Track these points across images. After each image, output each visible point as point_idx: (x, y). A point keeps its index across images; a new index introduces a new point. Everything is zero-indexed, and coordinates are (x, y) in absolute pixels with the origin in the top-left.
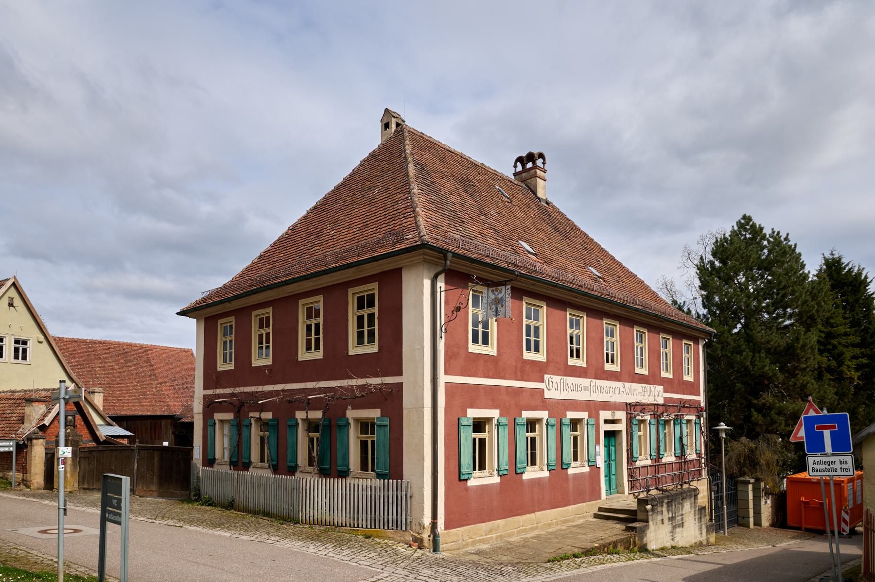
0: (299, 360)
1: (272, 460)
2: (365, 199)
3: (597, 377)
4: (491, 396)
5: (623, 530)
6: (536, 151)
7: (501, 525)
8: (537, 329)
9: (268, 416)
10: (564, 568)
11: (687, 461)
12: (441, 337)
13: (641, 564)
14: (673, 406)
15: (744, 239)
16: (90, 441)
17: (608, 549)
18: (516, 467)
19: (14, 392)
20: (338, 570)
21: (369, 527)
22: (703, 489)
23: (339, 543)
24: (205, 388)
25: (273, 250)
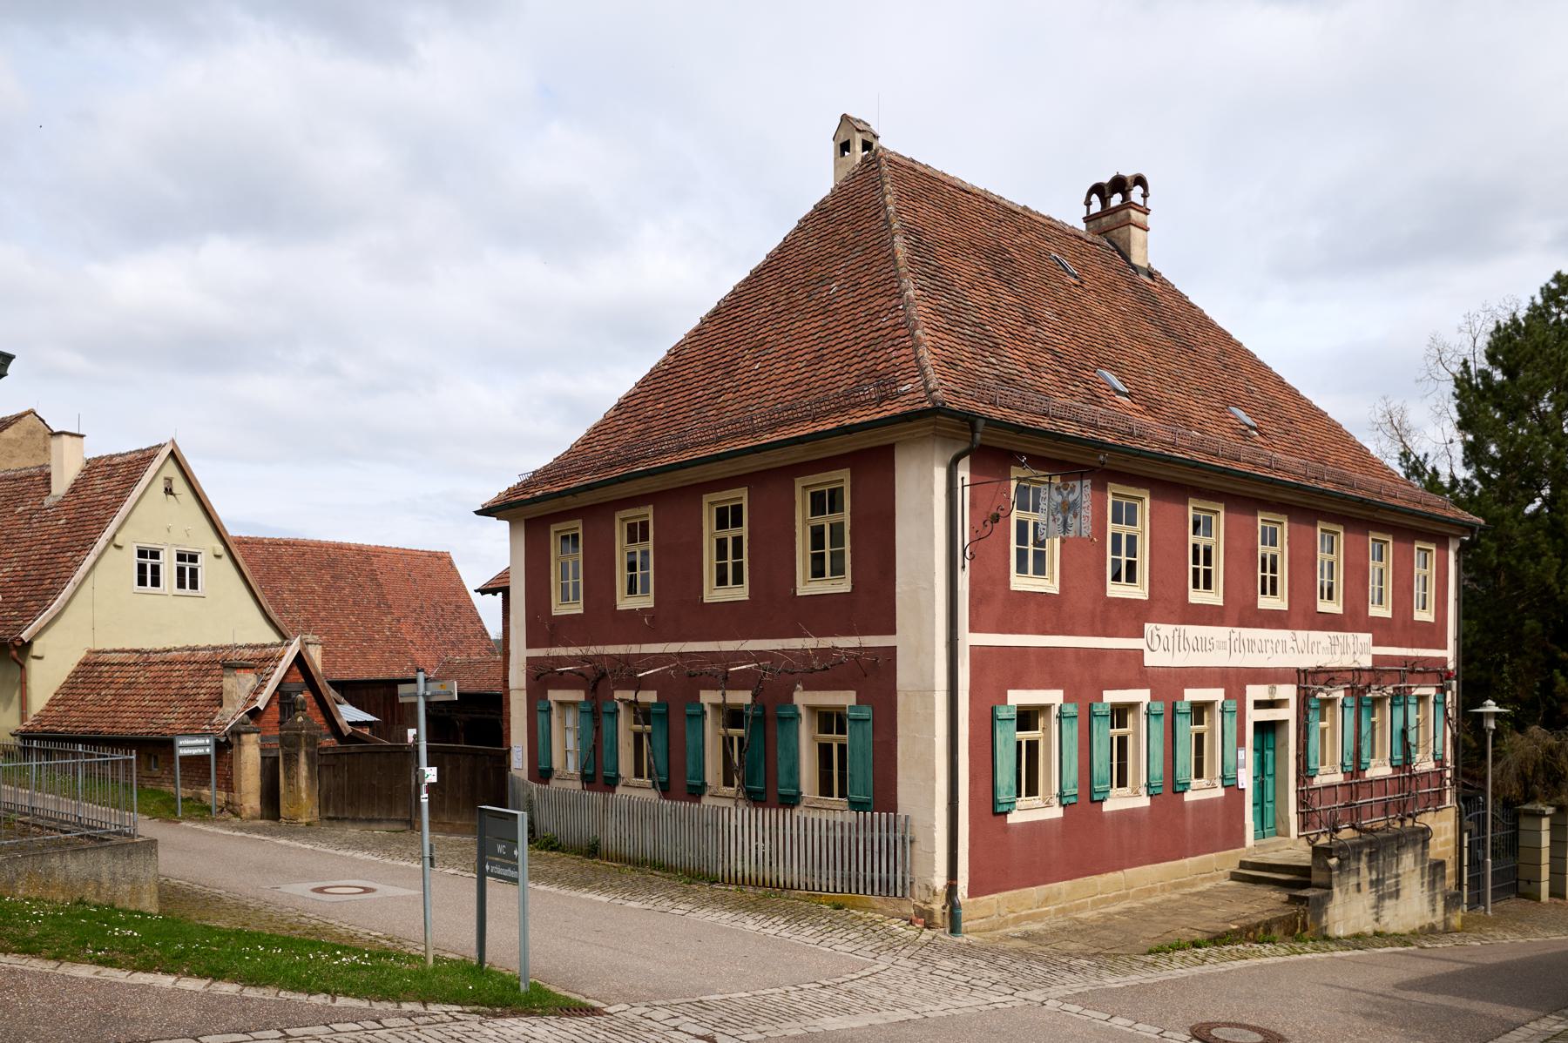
1: (659, 774)
2: (814, 302)
3: (1242, 624)
4: (1045, 668)
5: (1284, 902)
6: (1128, 173)
7: (1064, 891)
8: (1132, 540)
9: (649, 697)
10: (1176, 964)
11: (1415, 776)
13: (1314, 960)
14: (1389, 670)
15: (1555, 323)
16: (327, 736)
17: (1255, 933)
18: (1091, 791)
19: (194, 650)
20: (805, 957)
21: (839, 890)
22: (1446, 828)
23: (795, 916)
24: (530, 645)
25: (642, 394)
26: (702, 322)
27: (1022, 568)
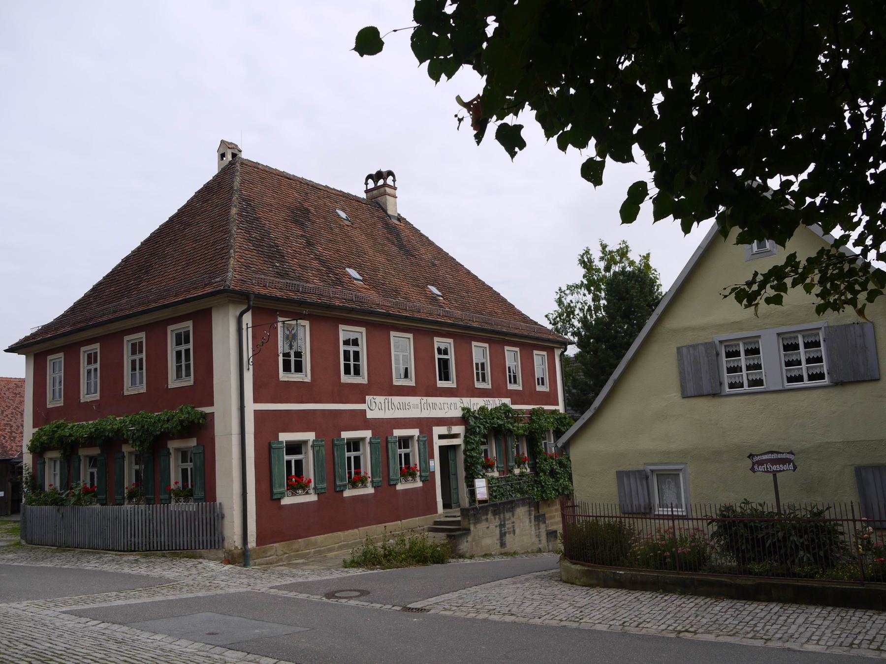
3: (428, 395)
8: (356, 354)
12: (249, 369)
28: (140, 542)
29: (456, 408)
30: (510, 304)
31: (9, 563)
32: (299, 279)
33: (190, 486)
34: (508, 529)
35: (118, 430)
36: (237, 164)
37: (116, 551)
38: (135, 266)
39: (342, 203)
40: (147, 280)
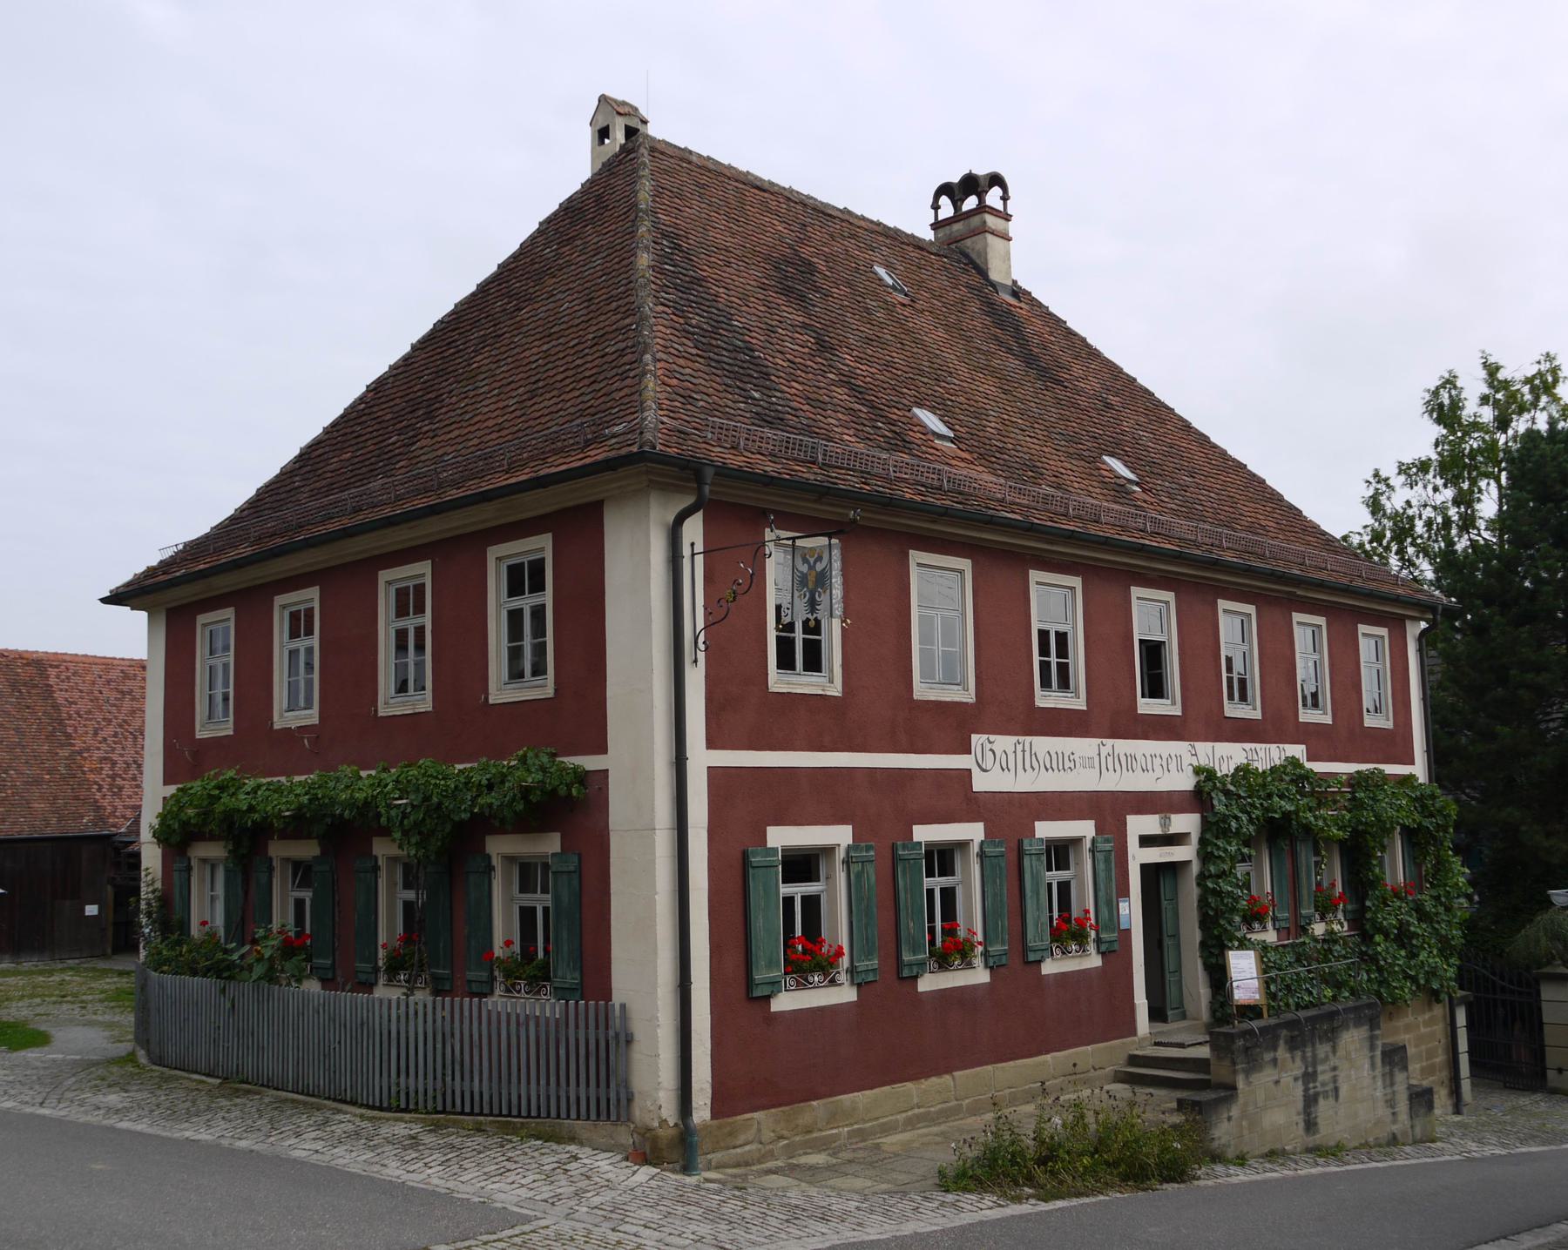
0: (380, 714)
6: (981, 170)
12: (696, 661)
26: (414, 347)
27: (1046, 684)
28: (421, 1089)
29: (1180, 769)
30: (1291, 507)
31: (111, 1122)
32: (809, 430)
33: (541, 954)
34: (1323, 1084)
35: (366, 803)
36: (642, 150)
37: (362, 1106)
38: (398, 401)
39: (885, 251)
40: (431, 434)
